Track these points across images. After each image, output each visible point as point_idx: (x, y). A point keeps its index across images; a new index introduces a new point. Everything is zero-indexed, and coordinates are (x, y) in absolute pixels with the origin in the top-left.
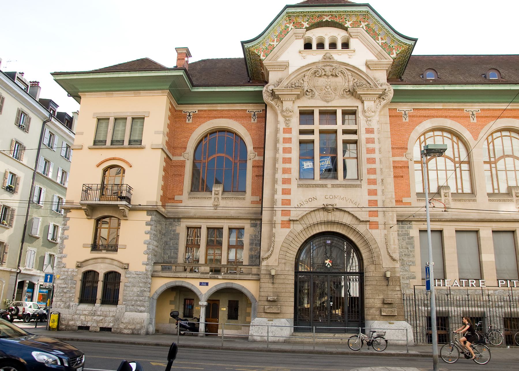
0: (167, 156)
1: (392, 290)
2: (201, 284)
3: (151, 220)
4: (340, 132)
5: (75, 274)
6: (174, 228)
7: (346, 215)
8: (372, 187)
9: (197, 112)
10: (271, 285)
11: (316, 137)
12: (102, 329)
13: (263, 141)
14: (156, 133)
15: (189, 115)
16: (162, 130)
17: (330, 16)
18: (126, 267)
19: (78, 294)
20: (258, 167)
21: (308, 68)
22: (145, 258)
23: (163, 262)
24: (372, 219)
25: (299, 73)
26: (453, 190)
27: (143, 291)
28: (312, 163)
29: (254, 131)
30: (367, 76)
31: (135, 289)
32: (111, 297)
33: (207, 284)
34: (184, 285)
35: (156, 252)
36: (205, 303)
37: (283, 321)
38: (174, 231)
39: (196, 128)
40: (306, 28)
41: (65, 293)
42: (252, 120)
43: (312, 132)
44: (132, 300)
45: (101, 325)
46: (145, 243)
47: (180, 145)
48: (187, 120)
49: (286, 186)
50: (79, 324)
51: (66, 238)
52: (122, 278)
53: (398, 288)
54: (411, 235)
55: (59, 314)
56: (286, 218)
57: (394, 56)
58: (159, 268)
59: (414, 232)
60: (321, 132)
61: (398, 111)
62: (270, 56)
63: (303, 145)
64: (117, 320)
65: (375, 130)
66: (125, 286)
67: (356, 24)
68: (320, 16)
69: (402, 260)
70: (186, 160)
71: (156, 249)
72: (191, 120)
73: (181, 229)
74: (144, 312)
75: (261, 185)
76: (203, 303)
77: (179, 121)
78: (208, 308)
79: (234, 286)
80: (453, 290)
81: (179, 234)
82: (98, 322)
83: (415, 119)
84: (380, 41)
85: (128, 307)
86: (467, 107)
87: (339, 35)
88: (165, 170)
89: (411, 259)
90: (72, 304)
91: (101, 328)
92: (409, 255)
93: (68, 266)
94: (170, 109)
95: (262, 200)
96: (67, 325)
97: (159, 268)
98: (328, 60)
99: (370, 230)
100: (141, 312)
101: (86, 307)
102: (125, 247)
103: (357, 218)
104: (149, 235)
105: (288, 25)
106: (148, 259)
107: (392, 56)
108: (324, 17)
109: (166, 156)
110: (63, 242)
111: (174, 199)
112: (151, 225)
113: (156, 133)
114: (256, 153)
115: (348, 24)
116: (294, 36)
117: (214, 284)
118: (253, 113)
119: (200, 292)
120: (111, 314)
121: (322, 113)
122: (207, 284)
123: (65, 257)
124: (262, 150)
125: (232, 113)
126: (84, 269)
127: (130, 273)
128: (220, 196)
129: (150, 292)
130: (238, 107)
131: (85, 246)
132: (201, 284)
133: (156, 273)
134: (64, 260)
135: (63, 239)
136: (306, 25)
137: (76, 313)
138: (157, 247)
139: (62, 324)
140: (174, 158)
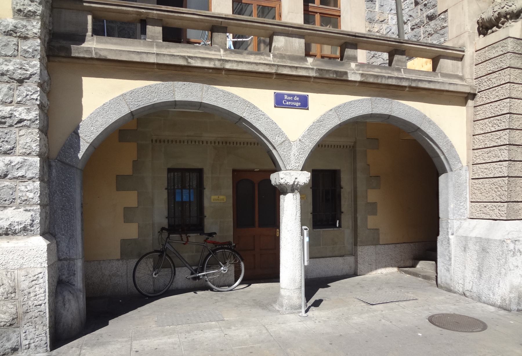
2: (279, 102)
33: (304, 104)
76: (292, 173)
117: (327, 109)
119: (281, 133)
122: (304, 104)
132: (279, 102)
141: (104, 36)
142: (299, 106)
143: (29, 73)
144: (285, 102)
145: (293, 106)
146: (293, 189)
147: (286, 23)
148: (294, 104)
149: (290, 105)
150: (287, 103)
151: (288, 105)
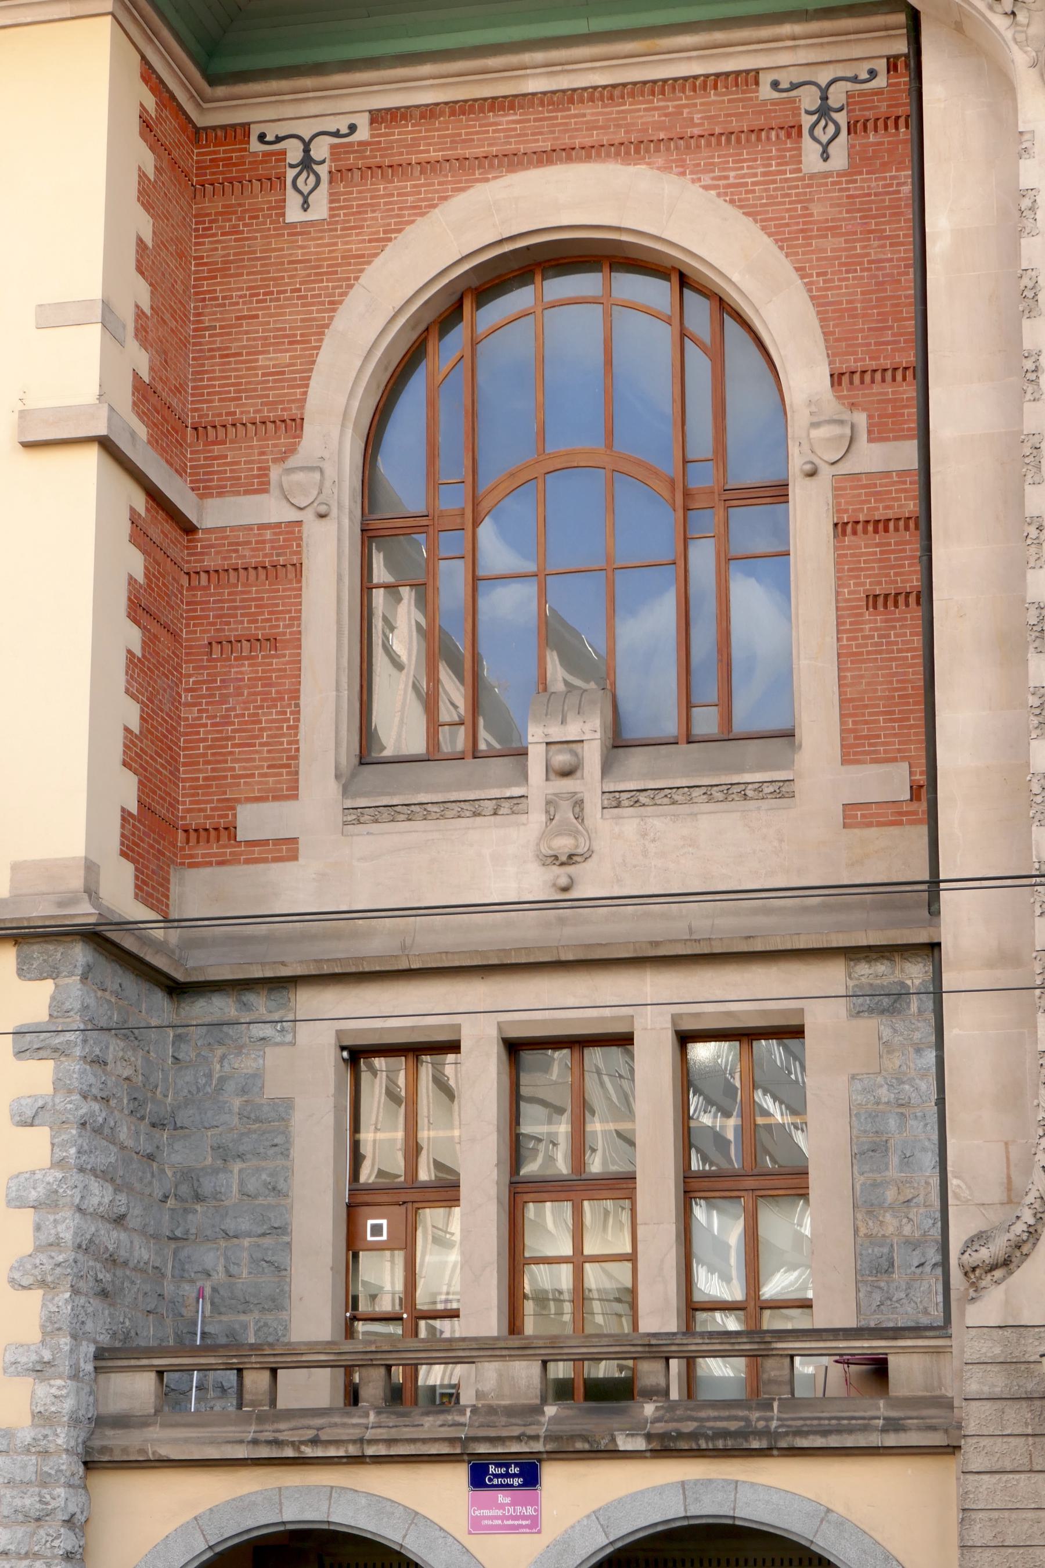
0: (154, 495)
3: (57, 1008)
6: (246, 1064)
9: (363, 134)
13: (909, 311)
14: (52, 317)
15: (307, 163)
16: (96, 292)
20: (881, 525)
29: (831, 243)
35: (112, 1261)
38: (251, 1084)
39: (364, 259)
42: (810, 150)
46: (17, 1202)
48: (293, 200)
58: (136, 1389)
61: (255, 146)
70: (308, 516)
75: (917, 677)
77: (227, 212)
81: (288, 1104)
86: (270, 113)
88: (140, 608)
94: (147, 125)
95: (926, 790)
97: (136, 1389)
104: (41, 1135)
109: (140, 501)
111: (230, 830)
112: (59, 1052)
113: (52, 317)
114: (861, 419)
118: (809, 99)
124: (909, 391)
125: (644, 115)
128: (590, 782)
130: (685, 60)
138: (119, 1220)
140: (214, 514)
141: (298, 848)
142: (520, 1485)
143: (50, 1507)
144: (490, 1480)
145: (508, 1485)
147: (678, 643)
148: (509, 1481)
149: (502, 1486)
150: (495, 1481)
151: (497, 1486)
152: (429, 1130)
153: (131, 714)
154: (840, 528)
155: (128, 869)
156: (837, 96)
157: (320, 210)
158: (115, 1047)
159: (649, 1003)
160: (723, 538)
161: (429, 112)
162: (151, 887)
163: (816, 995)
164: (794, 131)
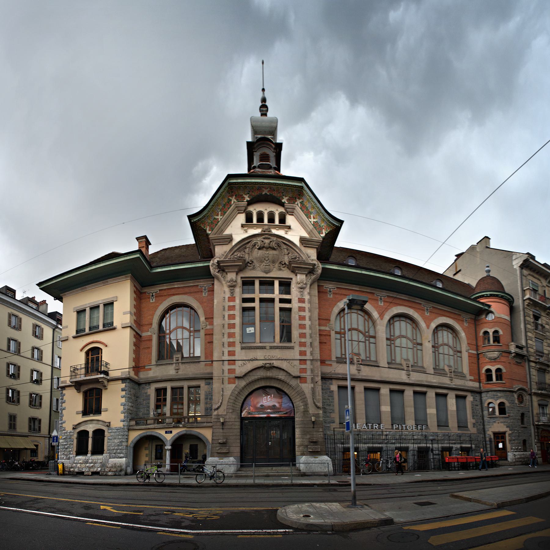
0: (136, 332)
1: (316, 431)
2: (166, 432)
3: (126, 386)
4: (277, 301)
5: (72, 434)
7: (282, 372)
8: (303, 349)
10: (221, 431)
11: (256, 304)
12: (94, 473)
15: (152, 296)
16: (129, 310)
17: (269, 189)
18: (108, 425)
19: (75, 449)
21: (248, 241)
22: (122, 416)
23: (135, 417)
24: (303, 375)
25: (242, 244)
26: (363, 357)
27: (121, 442)
28: (253, 328)
30: (300, 250)
31: (116, 441)
32: (98, 450)
33: (171, 432)
34: (153, 434)
36: (170, 447)
37: (232, 459)
38: (146, 393)
39: (158, 306)
40: (247, 201)
41: (67, 448)
43: (252, 300)
44: (114, 450)
45: (92, 470)
46: (121, 405)
47: (147, 323)
49: (231, 349)
50: (76, 470)
51: (64, 409)
52: (106, 433)
53: (321, 430)
54: (332, 389)
55: (63, 464)
56: (233, 376)
57: (323, 235)
58: (133, 423)
59: (334, 387)
60: (262, 300)
62: (215, 230)
63: (246, 313)
64: (103, 465)
65: (306, 300)
66: (108, 439)
67: (292, 200)
68: (259, 189)
69: (324, 408)
71: (131, 408)
72: (154, 299)
73: (151, 391)
74: (123, 457)
76: (168, 447)
78: (172, 451)
79: (192, 433)
80: (362, 431)
82: (90, 468)
83: (337, 296)
84: (312, 220)
85: (111, 455)
87: (277, 210)
89: (331, 408)
90: (71, 456)
91: (92, 472)
92: (330, 405)
93: (67, 429)
94: (135, 292)
96: (70, 471)
97: (133, 423)
98: (266, 234)
99: (300, 384)
100: (121, 458)
101: (81, 458)
102: (106, 410)
103: (290, 375)
104: (124, 399)
105: (231, 198)
106: (125, 417)
107: (322, 235)
108: (263, 189)
109: (135, 333)
110: (62, 412)
114: (208, 323)
115: (284, 200)
116: (236, 210)
117: (176, 432)
118: (204, 288)
120: (99, 461)
121: (262, 283)
122: (171, 432)
123: (64, 422)
125: (187, 290)
126: (78, 430)
127: (112, 429)
129: (127, 442)
131: (78, 413)
132: (166, 432)
133: (131, 427)
134: (64, 425)
135: (62, 410)
136: (247, 198)
137: (74, 463)
139: (65, 471)
146: (168, 450)
152: (533, 454)
153: (134, 356)
154: (205, 335)
155: (133, 372)
156: (206, 288)
157: (154, 301)
158: (132, 390)
159: (185, 384)
160: (194, 336)
161: (165, 289)
162: (137, 374)
163: (202, 383)
164: (202, 291)
